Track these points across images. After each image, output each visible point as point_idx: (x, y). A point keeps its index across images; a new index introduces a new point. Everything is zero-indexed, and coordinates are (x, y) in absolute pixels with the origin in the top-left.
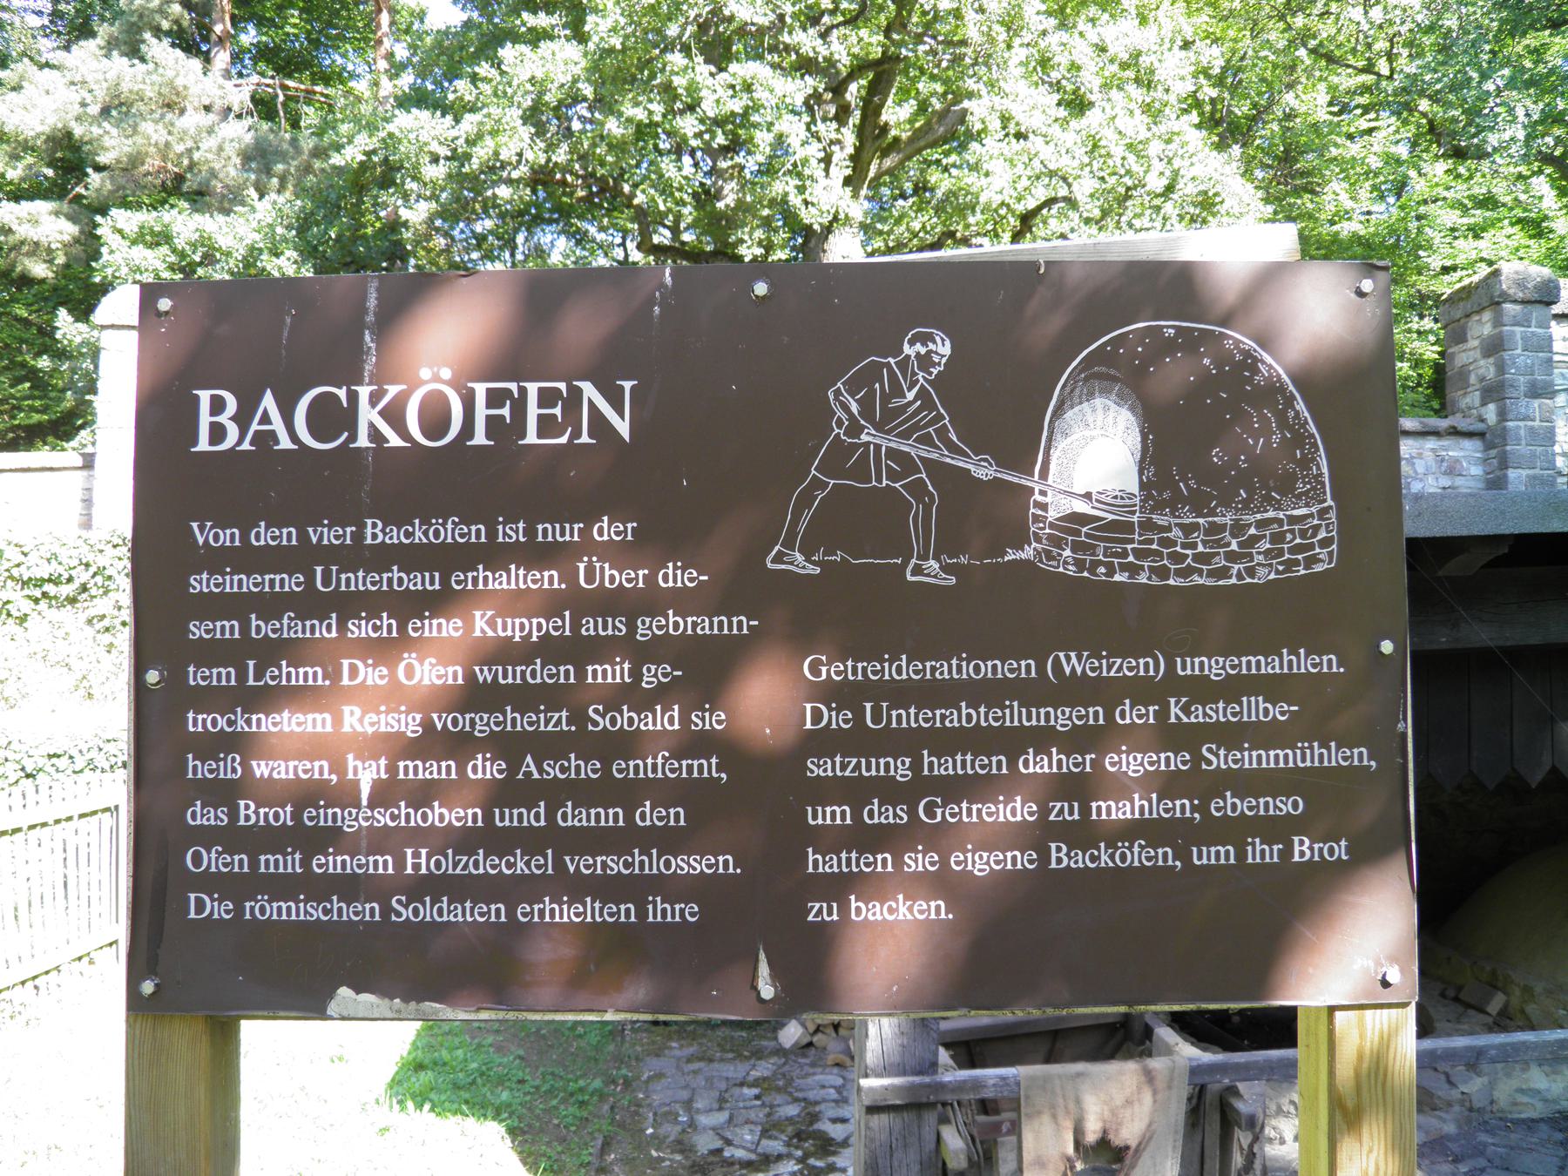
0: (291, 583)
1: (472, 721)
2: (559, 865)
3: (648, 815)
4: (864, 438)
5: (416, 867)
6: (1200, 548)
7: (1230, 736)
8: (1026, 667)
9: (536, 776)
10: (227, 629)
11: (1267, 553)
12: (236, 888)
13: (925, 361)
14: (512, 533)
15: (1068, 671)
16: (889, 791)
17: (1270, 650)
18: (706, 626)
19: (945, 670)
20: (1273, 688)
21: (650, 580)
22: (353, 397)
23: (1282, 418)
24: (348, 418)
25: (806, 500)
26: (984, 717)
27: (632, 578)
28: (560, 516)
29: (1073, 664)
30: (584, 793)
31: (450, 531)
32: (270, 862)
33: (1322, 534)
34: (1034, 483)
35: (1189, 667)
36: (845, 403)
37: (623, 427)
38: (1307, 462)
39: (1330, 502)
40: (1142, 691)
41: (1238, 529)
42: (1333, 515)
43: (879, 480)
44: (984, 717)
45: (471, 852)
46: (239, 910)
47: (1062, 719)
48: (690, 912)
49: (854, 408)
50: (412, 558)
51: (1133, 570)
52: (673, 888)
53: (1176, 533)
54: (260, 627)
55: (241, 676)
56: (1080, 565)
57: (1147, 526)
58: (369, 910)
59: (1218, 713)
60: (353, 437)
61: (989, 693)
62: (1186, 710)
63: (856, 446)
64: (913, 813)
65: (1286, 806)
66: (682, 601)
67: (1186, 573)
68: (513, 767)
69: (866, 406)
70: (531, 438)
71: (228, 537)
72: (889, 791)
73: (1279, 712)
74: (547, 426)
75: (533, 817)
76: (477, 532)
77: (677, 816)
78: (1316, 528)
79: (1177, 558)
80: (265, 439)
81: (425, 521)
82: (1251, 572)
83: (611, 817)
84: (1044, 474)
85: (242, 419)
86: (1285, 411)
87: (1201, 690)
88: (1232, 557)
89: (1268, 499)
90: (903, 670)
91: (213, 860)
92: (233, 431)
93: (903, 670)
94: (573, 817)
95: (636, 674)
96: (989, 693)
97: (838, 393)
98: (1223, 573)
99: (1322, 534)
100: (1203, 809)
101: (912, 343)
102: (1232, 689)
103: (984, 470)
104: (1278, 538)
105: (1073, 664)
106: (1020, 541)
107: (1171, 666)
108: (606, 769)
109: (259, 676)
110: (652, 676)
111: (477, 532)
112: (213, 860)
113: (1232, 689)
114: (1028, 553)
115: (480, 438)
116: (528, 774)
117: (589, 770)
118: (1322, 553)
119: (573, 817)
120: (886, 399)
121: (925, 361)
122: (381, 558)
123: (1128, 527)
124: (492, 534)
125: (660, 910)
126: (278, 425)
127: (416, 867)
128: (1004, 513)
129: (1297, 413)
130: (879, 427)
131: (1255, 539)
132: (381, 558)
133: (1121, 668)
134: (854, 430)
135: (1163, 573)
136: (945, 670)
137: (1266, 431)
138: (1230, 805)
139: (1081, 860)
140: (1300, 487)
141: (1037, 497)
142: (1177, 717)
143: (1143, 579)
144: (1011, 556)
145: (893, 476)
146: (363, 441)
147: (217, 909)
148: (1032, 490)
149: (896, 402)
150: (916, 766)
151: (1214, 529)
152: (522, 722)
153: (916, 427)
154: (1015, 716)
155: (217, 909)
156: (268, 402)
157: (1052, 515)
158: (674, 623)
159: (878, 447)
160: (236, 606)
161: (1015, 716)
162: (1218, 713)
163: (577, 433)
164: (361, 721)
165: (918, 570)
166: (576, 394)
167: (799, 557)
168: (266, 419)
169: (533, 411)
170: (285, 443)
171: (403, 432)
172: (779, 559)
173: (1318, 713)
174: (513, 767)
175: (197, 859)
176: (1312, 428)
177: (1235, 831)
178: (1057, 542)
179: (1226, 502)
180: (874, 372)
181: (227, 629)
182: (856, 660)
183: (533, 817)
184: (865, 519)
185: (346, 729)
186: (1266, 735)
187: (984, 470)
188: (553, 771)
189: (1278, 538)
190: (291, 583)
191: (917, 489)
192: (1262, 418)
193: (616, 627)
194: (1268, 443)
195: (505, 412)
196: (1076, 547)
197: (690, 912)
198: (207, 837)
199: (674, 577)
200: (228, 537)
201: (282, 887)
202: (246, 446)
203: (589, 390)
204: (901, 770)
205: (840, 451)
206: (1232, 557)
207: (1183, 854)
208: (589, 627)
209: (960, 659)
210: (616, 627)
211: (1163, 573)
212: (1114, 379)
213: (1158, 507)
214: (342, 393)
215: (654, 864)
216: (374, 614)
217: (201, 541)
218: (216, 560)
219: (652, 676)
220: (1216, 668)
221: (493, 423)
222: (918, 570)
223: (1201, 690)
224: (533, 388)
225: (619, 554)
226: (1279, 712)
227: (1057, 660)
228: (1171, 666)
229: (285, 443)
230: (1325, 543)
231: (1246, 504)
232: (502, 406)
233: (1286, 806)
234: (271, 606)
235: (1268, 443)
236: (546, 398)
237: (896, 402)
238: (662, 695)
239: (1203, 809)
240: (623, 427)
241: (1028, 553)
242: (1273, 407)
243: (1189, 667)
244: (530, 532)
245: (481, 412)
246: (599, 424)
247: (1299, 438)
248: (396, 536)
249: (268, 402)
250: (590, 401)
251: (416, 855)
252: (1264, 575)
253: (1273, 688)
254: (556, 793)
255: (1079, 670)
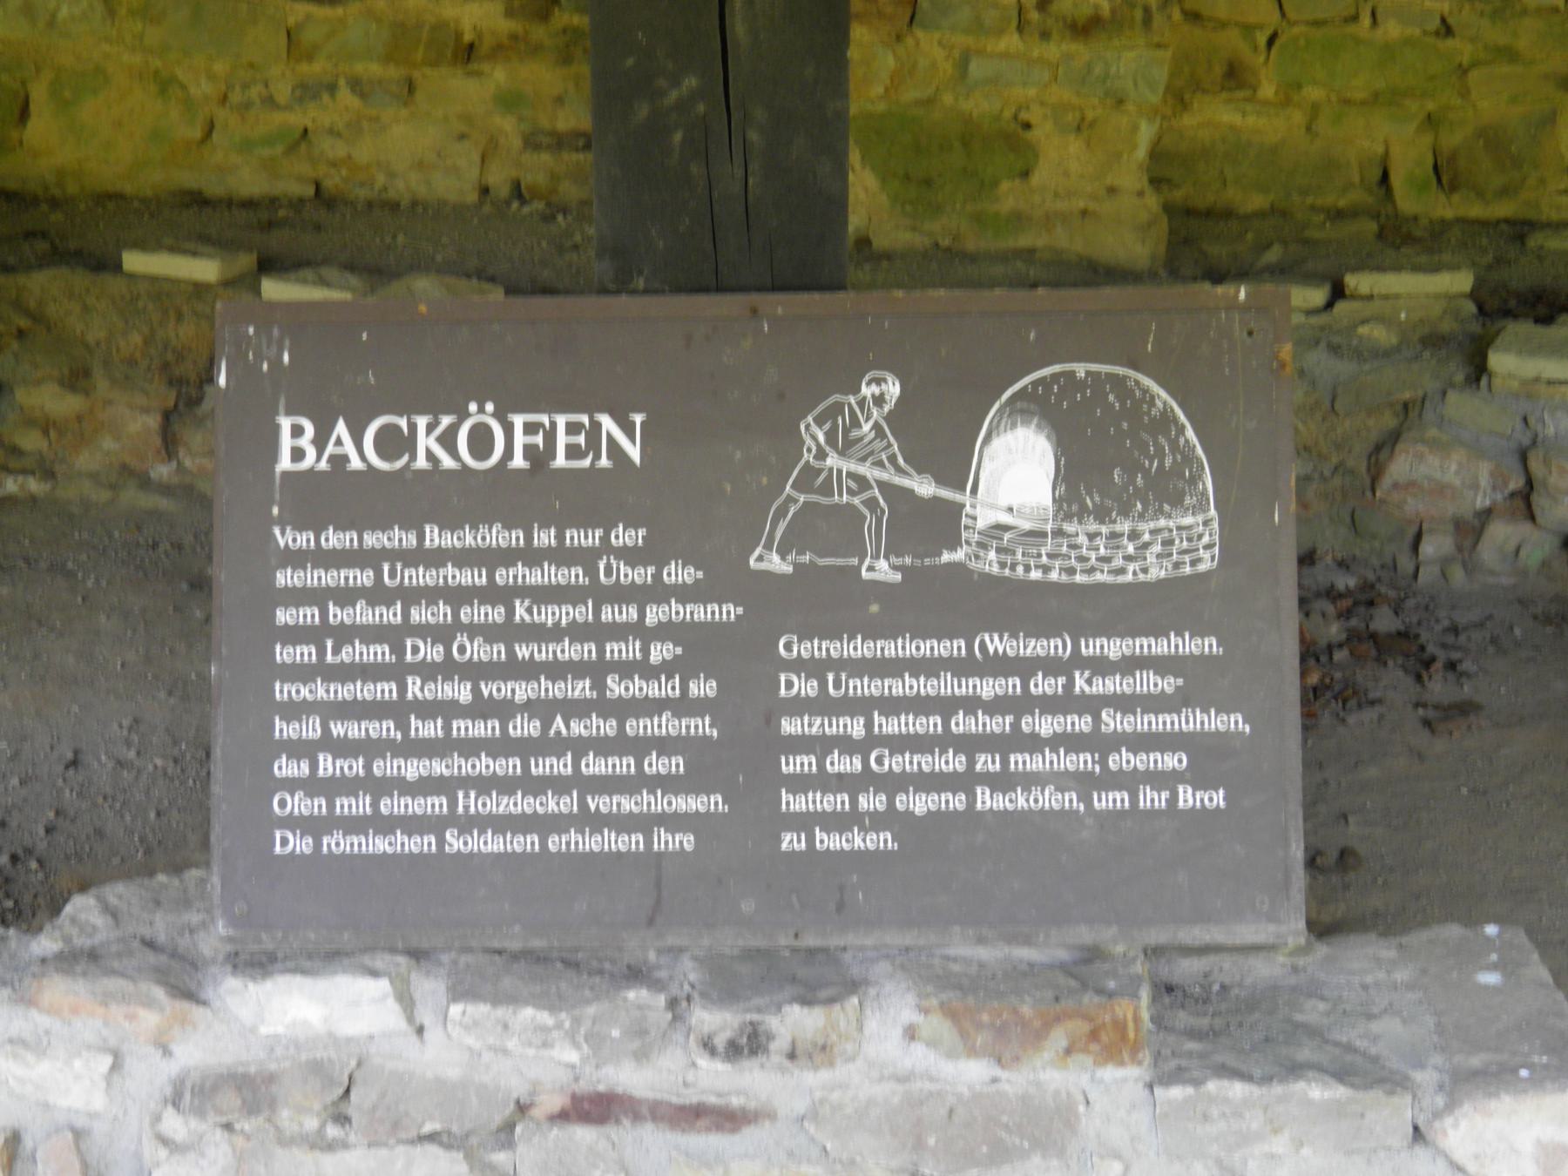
0: (365, 578)
1: (513, 691)
2: (583, 804)
3: (656, 765)
4: (829, 462)
5: (466, 808)
6: (1102, 551)
7: (1125, 703)
8: (958, 647)
9: (564, 731)
10: (308, 615)
11: (1159, 556)
12: (313, 827)
13: (879, 400)
14: (545, 538)
15: (991, 651)
16: (846, 745)
17: (1159, 632)
18: (700, 613)
19: (890, 649)
20: (1161, 665)
21: (657, 576)
22: (413, 427)
23: (1175, 447)
24: (409, 444)
25: (781, 513)
26: (926, 687)
27: (641, 575)
28: (585, 524)
29: (996, 644)
30: (603, 747)
31: (496, 536)
32: (346, 805)
33: (1206, 539)
34: (966, 498)
35: (1090, 647)
36: (813, 433)
37: (634, 452)
38: (1195, 479)
39: (1213, 512)
40: (1051, 666)
41: (1134, 535)
42: (1216, 525)
43: (841, 495)
44: (926, 687)
45: (512, 793)
46: (318, 845)
47: (988, 688)
48: (688, 841)
49: (821, 438)
50: (464, 558)
51: (1046, 569)
52: (674, 822)
53: (1082, 539)
54: (336, 615)
55: (321, 652)
56: (1002, 565)
57: (1059, 533)
58: (428, 843)
59: (1111, 685)
60: (413, 457)
61: (928, 667)
62: (1089, 682)
63: (820, 471)
64: (866, 762)
65: (1172, 761)
66: (685, 594)
67: (1091, 570)
68: (546, 725)
69: (831, 437)
70: (560, 461)
71: (304, 540)
72: (846, 745)
73: (1168, 684)
74: (573, 452)
75: (561, 766)
76: (516, 537)
77: (677, 764)
78: (1200, 537)
79: (1082, 559)
80: (340, 461)
81: (475, 527)
82: (1145, 571)
83: (624, 765)
84: (974, 490)
85: (320, 442)
86: (1177, 437)
87: (1101, 666)
88: (1128, 558)
89: (1161, 511)
90: (860, 648)
91: (299, 804)
92: (311, 453)
93: (860, 648)
94: (594, 766)
95: (646, 651)
96: (928, 667)
97: (808, 427)
98: (1122, 571)
99: (1206, 539)
100: (1103, 762)
101: (869, 384)
102: (1130, 665)
103: (925, 488)
104: (1168, 543)
105: (996, 644)
106: (954, 544)
107: (1076, 646)
108: (621, 726)
109: (336, 651)
110: (660, 652)
111: (516, 537)
112: (299, 804)
113: (1130, 665)
114: (959, 555)
115: (519, 461)
116: (558, 733)
117: (609, 728)
118: (1206, 555)
119: (594, 766)
120: (846, 431)
121: (879, 400)
122: (437, 558)
123: (1043, 534)
124: (529, 538)
125: (664, 840)
126: (349, 448)
127: (466, 808)
128: (943, 523)
129: (1187, 441)
130: (842, 453)
131: (1146, 546)
132: (437, 558)
133: (1035, 647)
134: (821, 455)
135: (1071, 571)
136: (890, 649)
137: (1160, 454)
138: (1122, 760)
139: (1000, 802)
140: (1188, 501)
141: (968, 509)
142: (430, 456)
143: (1054, 576)
144: (946, 557)
145: (851, 492)
146: (421, 462)
147: (301, 844)
148: (964, 506)
149: (855, 434)
150: (869, 725)
151: (1114, 535)
152: (557, 690)
153: (872, 453)
154: (947, 685)
155: (301, 844)
156: (341, 428)
157: (981, 524)
158: (676, 611)
159: (840, 472)
160: (317, 597)
161: (947, 685)
162: (1111, 685)
163: (597, 456)
164: (422, 689)
165: (871, 569)
166: (596, 426)
167: (776, 558)
168: (339, 442)
169: (562, 440)
170: (356, 463)
171: (454, 454)
172: (760, 559)
173: (1199, 684)
174: (546, 725)
175: (283, 804)
176: (1199, 451)
177: (1129, 781)
178: (983, 546)
179: (1125, 512)
180: (838, 408)
181: (308, 615)
182: (821, 639)
183: (561, 766)
184: (830, 527)
185: (410, 696)
186: (1155, 703)
187: (925, 488)
188: (577, 728)
189: (1168, 543)
190: (365, 578)
191: (871, 504)
192: (1156, 443)
193: (630, 613)
194: (1161, 464)
195: (539, 439)
196: (998, 551)
197: (688, 841)
198: (292, 785)
199: (679, 574)
200: (304, 540)
201: (354, 825)
202: (323, 465)
203: (607, 423)
204: (857, 729)
205: (810, 472)
206: (1128, 558)
207: (1086, 798)
208: (607, 614)
209: (904, 638)
210: (630, 613)
211: (1071, 571)
212: (1033, 414)
213: (1068, 517)
214: (403, 423)
215: (657, 803)
216: (432, 602)
217: (282, 543)
218: (296, 559)
219: (660, 652)
220: (1115, 648)
221: (529, 450)
222: (871, 569)
223: (1101, 666)
224: (561, 421)
225: (631, 556)
226: (1168, 684)
227: (982, 643)
228: (1076, 646)
229: (356, 463)
230: (1208, 547)
231: (1141, 516)
232: (537, 433)
233: (1172, 761)
234: (346, 596)
235: (1161, 464)
236: (573, 429)
237: (855, 434)
238: (668, 669)
239: (1103, 762)
240: (634, 452)
241: (959, 555)
242: (1167, 434)
243: (1090, 647)
244: (560, 537)
245: (520, 439)
246: (615, 449)
247: (1188, 457)
248: (449, 540)
249: (341, 428)
250: (609, 435)
251: (467, 796)
252: (1156, 573)
253: (1161, 665)
254: (580, 747)
255: (1001, 651)
